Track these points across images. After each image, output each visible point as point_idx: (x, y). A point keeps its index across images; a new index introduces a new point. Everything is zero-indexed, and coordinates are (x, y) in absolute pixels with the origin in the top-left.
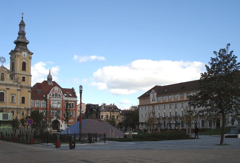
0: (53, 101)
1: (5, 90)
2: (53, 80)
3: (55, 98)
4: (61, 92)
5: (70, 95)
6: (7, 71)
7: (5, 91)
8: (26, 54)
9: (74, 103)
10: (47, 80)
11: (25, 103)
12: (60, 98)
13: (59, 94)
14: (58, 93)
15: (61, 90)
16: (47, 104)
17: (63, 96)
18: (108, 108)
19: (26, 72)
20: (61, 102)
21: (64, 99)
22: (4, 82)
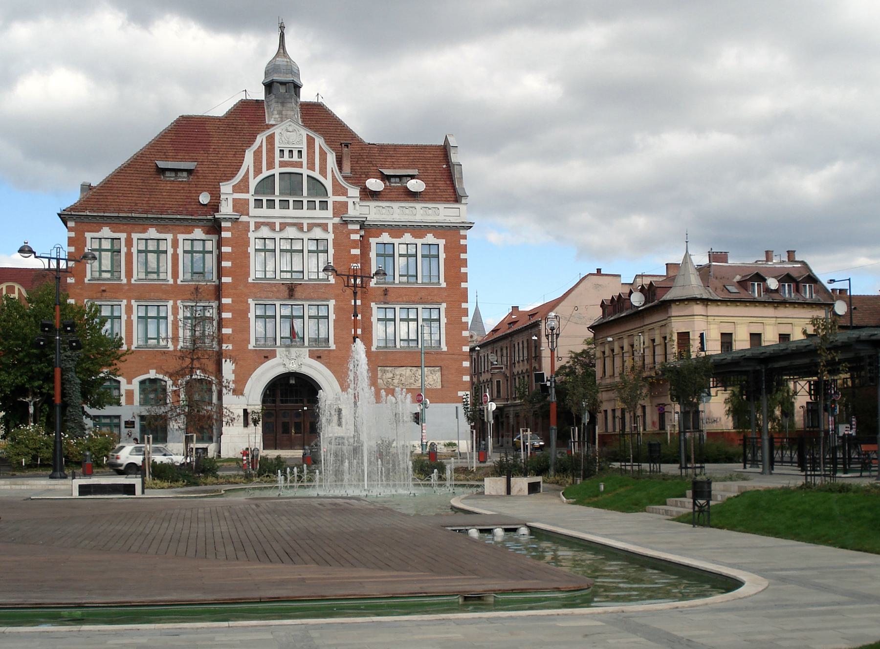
0: (265, 232)
2: (307, 95)
3: (277, 211)
4: (331, 159)
5: (415, 185)
9: (442, 242)
10: (263, 98)
12: (324, 205)
13: (316, 174)
14: (305, 171)
15: (326, 148)
16: (220, 258)
17: (344, 193)
18: (738, 278)
20: (331, 237)
21: (353, 212)
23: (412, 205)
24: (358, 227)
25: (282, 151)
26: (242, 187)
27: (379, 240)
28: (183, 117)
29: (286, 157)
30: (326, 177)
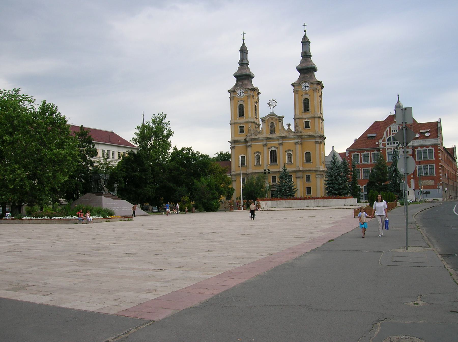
1: (277, 146)
3: (392, 145)
6: (278, 118)
7: (277, 148)
8: (238, 91)
9: (433, 148)
11: (311, 162)
19: (310, 113)
22: (274, 135)
23: (425, 140)
24: (411, 147)
25: (393, 131)
26: (384, 140)
27: (418, 149)
28: (376, 123)
29: (394, 132)
30: (387, 137)
